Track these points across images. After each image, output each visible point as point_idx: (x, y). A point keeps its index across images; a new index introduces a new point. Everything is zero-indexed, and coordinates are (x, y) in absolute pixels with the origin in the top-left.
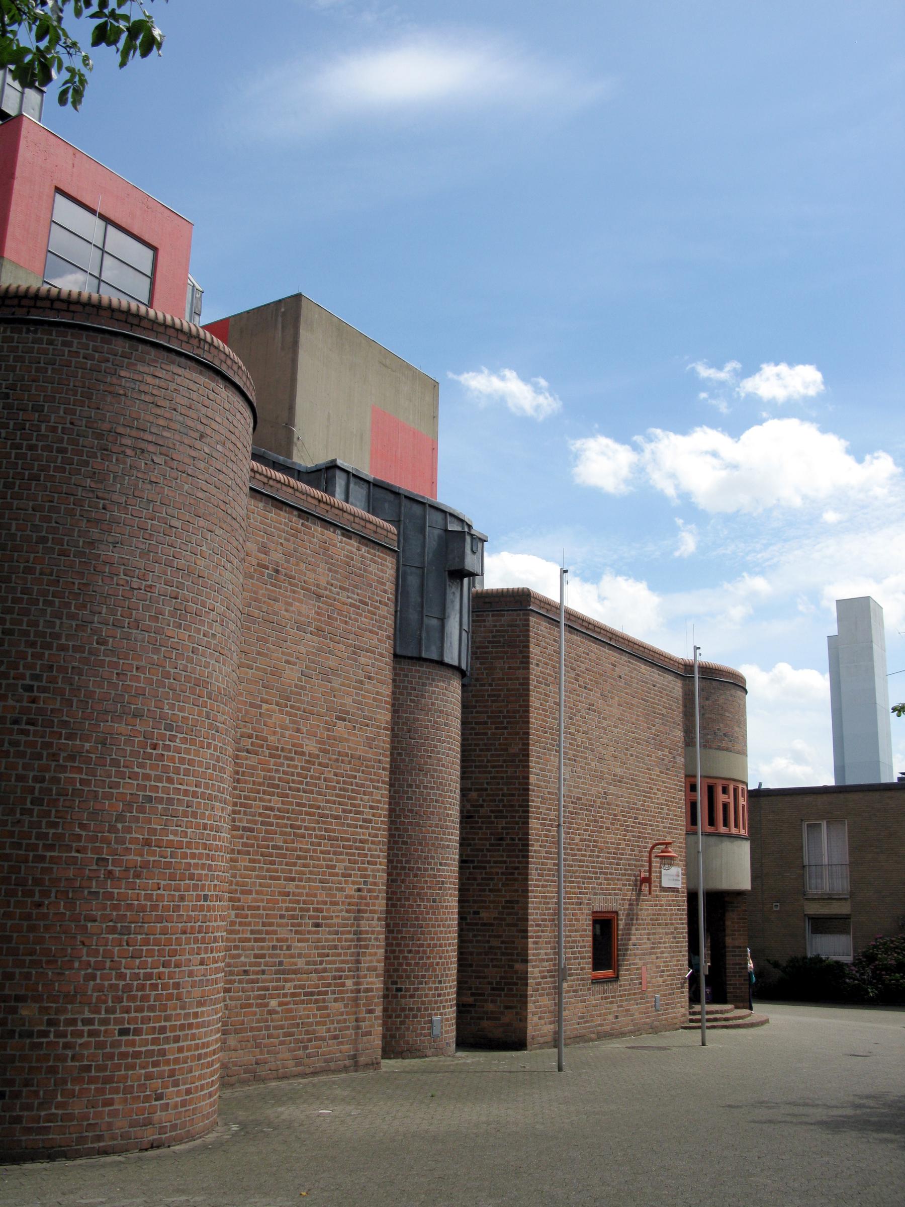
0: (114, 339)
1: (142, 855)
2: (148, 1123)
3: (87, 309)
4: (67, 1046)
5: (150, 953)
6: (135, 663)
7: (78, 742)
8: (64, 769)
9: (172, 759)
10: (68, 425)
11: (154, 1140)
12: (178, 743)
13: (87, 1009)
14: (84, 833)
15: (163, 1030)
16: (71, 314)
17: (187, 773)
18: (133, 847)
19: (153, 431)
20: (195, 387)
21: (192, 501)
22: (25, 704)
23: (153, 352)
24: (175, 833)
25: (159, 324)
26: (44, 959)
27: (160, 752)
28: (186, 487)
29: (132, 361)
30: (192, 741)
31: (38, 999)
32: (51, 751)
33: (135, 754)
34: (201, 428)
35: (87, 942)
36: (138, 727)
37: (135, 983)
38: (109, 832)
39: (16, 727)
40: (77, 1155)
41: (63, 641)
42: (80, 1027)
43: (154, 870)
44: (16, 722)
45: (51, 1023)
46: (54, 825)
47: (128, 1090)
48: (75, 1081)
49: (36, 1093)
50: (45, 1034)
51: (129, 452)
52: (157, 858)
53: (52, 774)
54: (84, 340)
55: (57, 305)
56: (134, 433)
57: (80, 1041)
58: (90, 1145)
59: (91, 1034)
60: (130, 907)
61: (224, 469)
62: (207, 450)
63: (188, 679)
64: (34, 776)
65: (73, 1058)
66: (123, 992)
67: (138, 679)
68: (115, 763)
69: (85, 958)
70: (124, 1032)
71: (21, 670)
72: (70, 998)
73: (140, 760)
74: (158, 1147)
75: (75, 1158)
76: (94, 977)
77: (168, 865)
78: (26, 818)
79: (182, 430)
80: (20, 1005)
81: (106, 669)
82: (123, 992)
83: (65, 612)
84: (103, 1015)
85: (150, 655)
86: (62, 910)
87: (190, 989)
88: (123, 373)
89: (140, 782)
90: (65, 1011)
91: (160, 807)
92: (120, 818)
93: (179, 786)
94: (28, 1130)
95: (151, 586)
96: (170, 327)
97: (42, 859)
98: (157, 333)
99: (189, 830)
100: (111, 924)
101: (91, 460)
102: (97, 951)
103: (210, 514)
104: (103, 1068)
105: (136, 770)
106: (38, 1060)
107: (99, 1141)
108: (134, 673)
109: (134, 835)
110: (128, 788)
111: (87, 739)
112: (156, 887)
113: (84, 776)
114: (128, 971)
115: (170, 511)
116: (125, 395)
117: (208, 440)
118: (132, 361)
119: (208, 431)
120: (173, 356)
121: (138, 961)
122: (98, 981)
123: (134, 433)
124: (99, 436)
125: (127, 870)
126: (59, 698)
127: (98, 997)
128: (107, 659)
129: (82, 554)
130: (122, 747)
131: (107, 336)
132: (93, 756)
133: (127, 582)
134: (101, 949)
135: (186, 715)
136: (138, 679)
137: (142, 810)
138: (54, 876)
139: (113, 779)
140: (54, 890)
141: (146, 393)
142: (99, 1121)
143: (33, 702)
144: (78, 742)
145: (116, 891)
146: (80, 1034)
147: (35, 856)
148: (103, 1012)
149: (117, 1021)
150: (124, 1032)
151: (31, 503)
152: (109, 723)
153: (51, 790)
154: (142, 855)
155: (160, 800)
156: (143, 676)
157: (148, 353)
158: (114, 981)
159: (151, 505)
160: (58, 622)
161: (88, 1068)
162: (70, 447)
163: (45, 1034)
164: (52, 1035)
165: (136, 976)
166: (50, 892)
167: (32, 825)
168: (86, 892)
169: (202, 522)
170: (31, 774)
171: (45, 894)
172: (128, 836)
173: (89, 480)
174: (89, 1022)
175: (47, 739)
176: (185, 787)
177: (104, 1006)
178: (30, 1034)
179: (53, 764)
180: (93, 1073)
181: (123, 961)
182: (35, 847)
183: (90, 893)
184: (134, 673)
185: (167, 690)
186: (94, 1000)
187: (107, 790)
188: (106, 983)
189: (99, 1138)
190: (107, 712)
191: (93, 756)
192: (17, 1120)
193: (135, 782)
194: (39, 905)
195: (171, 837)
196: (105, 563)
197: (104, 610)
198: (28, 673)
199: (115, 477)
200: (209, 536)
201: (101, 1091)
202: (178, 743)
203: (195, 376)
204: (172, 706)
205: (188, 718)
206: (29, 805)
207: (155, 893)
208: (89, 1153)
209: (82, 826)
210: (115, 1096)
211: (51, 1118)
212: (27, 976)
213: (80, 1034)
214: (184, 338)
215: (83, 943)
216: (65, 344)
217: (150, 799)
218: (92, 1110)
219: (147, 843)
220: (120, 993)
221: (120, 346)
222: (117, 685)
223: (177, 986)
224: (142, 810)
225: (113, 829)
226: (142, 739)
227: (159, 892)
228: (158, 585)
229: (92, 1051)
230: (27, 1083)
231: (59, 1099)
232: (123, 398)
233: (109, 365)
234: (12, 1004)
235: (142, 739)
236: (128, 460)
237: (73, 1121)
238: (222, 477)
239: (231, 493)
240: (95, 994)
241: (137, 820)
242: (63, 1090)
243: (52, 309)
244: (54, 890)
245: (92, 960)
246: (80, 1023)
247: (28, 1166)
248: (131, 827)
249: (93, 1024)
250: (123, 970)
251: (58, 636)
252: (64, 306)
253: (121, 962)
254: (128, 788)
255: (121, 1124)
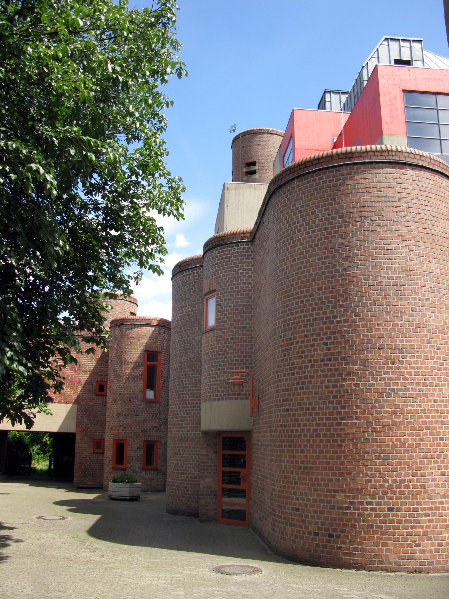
0: (341, 168)
1: (392, 419)
2: (411, 558)
3: (327, 159)
4: (359, 515)
5: (403, 469)
6: (376, 323)
7: (351, 366)
8: (345, 380)
9: (406, 368)
10: (327, 216)
11: (416, 568)
12: (408, 359)
13: (368, 497)
14: (358, 410)
15: (416, 510)
16: (320, 164)
17: (417, 374)
18: (386, 415)
19: (369, 205)
20: (388, 176)
21: (399, 234)
22: (325, 352)
23: (362, 167)
24: (413, 406)
25: (363, 153)
26: (345, 472)
27: (397, 365)
28: (394, 227)
29: (352, 175)
30: (419, 357)
31: (344, 491)
32: (339, 372)
33: (382, 368)
34: (398, 195)
35: (365, 464)
36: (382, 354)
37: (395, 484)
38: (371, 408)
39: (322, 363)
40: (370, 569)
41: (339, 319)
42: (365, 506)
43: (401, 426)
44: (322, 361)
45: (351, 503)
46: (344, 407)
47: (397, 539)
48: (366, 532)
49: (347, 536)
50: (348, 508)
51: (358, 220)
52: (401, 420)
53: (340, 383)
54: (328, 174)
55: (314, 163)
56: (359, 210)
57: (366, 513)
58: (377, 565)
59: (372, 509)
60: (387, 446)
61: (420, 211)
62: (404, 205)
63: (411, 325)
64: (333, 385)
65: (364, 521)
66: (388, 489)
67: (378, 330)
68: (371, 374)
69: (365, 472)
70: (390, 509)
71: (322, 336)
72: (359, 491)
73: (385, 371)
74: (420, 572)
75: (370, 571)
76: (371, 482)
77: (409, 423)
78: (331, 405)
79: (386, 200)
80: (336, 494)
81: (361, 328)
82: (388, 489)
83: (338, 304)
84: (377, 500)
85: (385, 317)
86: (351, 448)
87: (434, 488)
88: (348, 183)
89: (386, 382)
90: (357, 498)
91: (400, 393)
92: (377, 401)
93: (412, 381)
94: (345, 554)
95: (380, 282)
96: (369, 151)
97: (339, 424)
98: (363, 157)
99: (422, 404)
100: (377, 454)
101: (339, 229)
102: (371, 468)
103: (413, 237)
104: (381, 527)
105: (383, 376)
106: (347, 521)
107: (382, 564)
108: (377, 327)
109: (386, 409)
110: (379, 385)
111: (354, 364)
112: (403, 435)
113: (356, 382)
114: (390, 478)
115: (385, 242)
116: (351, 193)
117: (404, 200)
118: (352, 175)
119: (404, 195)
120: (374, 165)
121: (395, 473)
122: (373, 483)
123: (359, 210)
124: (342, 217)
125: (384, 427)
126: (339, 346)
127: (374, 491)
128: (361, 323)
129: (342, 275)
130: (374, 365)
131: (338, 168)
132: (359, 372)
133: (366, 283)
134: (373, 467)
135: (412, 344)
136: (378, 330)
137: (389, 395)
138: (346, 432)
139: (371, 382)
140: (347, 439)
141: (362, 188)
142: (380, 554)
143: (329, 350)
144: (351, 366)
145: (378, 438)
146: (366, 509)
147: (336, 423)
148: (377, 499)
149: (385, 504)
150: (390, 509)
151: (317, 257)
152: (366, 355)
153: (341, 391)
154: (392, 419)
155: (400, 390)
156: (381, 328)
157: (360, 168)
158: (382, 483)
159: (374, 242)
160: (335, 310)
161: (372, 527)
162: (329, 226)
163: (348, 508)
164: (352, 509)
165: (396, 481)
166: (345, 439)
167: (334, 408)
168: (362, 439)
169: (407, 243)
170: (331, 384)
171: (343, 441)
172: (383, 410)
173: (340, 239)
174: (371, 503)
175: (336, 367)
176: (417, 381)
177: (377, 496)
178: (342, 508)
179: (340, 378)
180: (375, 529)
181: (386, 473)
182: (336, 419)
183: (364, 439)
184: (377, 327)
185: (397, 333)
186: (372, 493)
187: (368, 388)
188: (378, 484)
189: (382, 562)
190: (363, 350)
191: (359, 372)
192: (340, 548)
193: (384, 382)
194: (341, 446)
195: (410, 408)
196: (354, 277)
197: (356, 300)
198: (325, 337)
199: (352, 234)
200: (414, 248)
201: (381, 539)
202: (408, 359)
203: (389, 170)
204: (402, 341)
205: (413, 345)
206: (331, 399)
207: (402, 438)
208: (377, 569)
209: (357, 407)
210: (389, 542)
211: (355, 549)
212: (338, 480)
213: (366, 509)
214: (379, 154)
215: (363, 464)
216: (320, 179)
217: (393, 390)
218: (376, 548)
219: (395, 412)
220: (386, 489)
221: (344, 171)
222: (367, 335)
223: (423, 486)
224: (389, 395)
225: (373, 407)
226: (385, 360)
227: (405, 437)
228: (384, 281)
229: (373, 518)
230: (343, 531)
231: (358, 540)
232: (350, 195)
233: (341, 181)
234: (333, 493)
235: (385, 360)
236: (358, 224)
237: (366, 552)
238: (418, 216)
239: (428, 222)
240: (372, 490)
241: (387, 401)
242: (360, 536)
243: (312, 165)
244: (347, 439)
245: (369, 472)
246: (365, 504)
247: (345, 571)
248: (384, 405)
249: (373, 505)
250: (387, 478)
251: (335, 317)
252: (317, 162)
253: (385, 474)
254: (379, 385)
255: (393, 557)
